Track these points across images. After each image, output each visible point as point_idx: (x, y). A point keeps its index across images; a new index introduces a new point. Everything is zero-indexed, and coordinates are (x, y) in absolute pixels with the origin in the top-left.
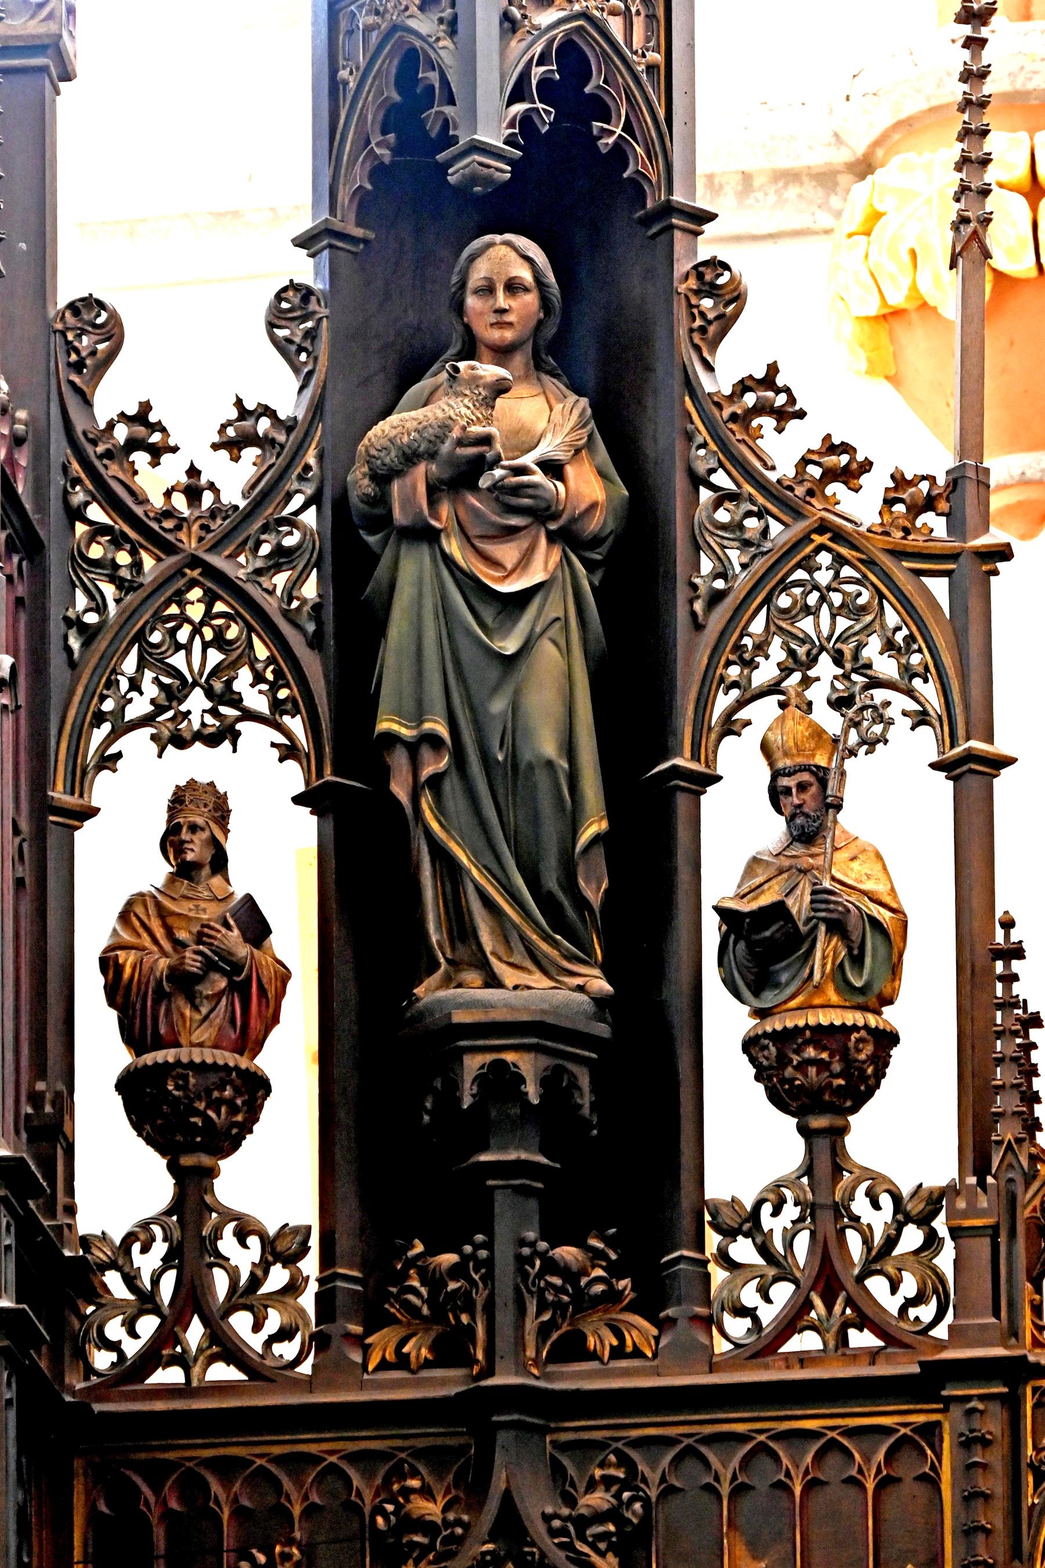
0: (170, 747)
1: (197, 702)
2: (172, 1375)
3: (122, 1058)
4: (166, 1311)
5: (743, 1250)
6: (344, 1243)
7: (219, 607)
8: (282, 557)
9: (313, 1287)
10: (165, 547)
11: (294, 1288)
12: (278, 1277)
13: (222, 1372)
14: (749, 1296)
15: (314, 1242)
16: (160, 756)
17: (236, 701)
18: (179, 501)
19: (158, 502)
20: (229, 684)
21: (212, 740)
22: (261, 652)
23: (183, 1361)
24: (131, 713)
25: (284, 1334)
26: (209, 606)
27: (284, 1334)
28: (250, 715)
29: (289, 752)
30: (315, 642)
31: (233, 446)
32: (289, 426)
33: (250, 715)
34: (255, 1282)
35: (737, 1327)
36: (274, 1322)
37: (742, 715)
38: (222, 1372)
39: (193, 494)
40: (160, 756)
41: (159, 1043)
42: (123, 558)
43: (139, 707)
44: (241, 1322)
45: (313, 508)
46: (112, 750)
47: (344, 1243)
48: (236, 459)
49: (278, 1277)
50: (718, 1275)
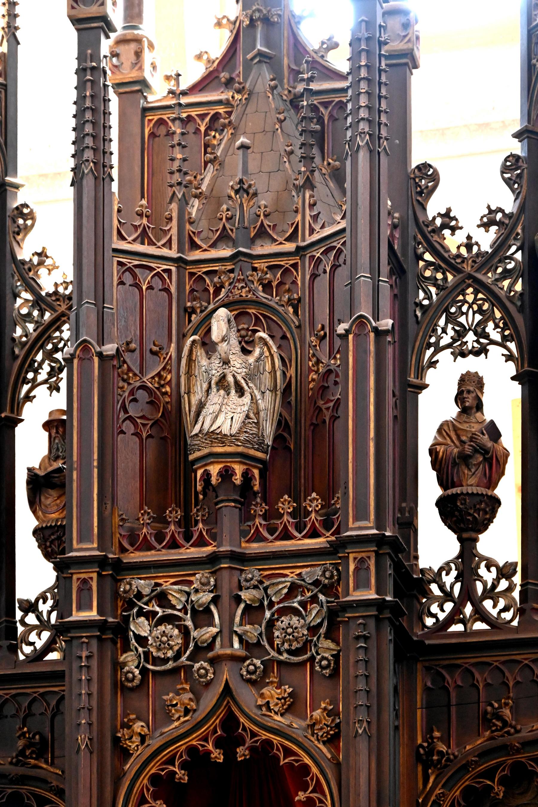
0: (459, 357)
1: (470, 337)
2: (458, 628)
3: (438, 492)
4: (456, 600)
5: (31, 619)
6: (531, 570)
7: (480, 296)
8: (507, 274)
9: (518, 588)
10: (456, 270)
11: (510, 588)
12: (504, 584)
13: (479, 626)
14: (33, 637)
15: (519, 569)
16: (455, 361)
17: (487, 336)
18: (463, 251)
19: (454, 251)
20: (484, 329)
21: (476, 353)
22: (498, 315)
23: (463, 621)
24: (443, 343)
25: (506, 609)
26: (476, 296)
27: (506, 609)
28: (493, 342)
29: (509, 358)
30: (521, 310)
31: (486, 226)
32: (510, 216)
33: (493, 342)
34: (494, 586)
35: (28, 649)
36: (502, 603)
37: (434, 359)
38: (479, 626)
39: (469, 246)
40: (455, 361)
41: (454, 486)
42: (439, 276)
43: (446, 340)
44: (488, 604)
45: (520, 252)
46: (434, 359)
47: (531, 570)
48: (487, 231)
49: (504, 584)
50: (20, 629)
